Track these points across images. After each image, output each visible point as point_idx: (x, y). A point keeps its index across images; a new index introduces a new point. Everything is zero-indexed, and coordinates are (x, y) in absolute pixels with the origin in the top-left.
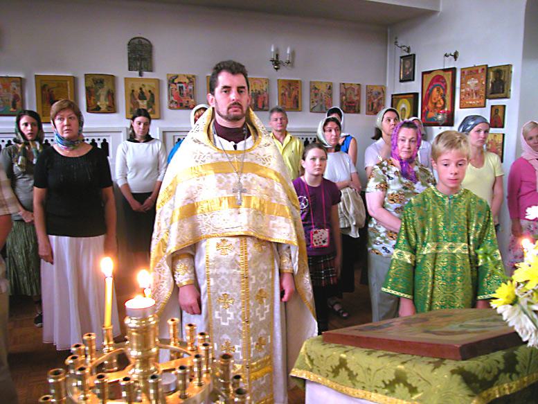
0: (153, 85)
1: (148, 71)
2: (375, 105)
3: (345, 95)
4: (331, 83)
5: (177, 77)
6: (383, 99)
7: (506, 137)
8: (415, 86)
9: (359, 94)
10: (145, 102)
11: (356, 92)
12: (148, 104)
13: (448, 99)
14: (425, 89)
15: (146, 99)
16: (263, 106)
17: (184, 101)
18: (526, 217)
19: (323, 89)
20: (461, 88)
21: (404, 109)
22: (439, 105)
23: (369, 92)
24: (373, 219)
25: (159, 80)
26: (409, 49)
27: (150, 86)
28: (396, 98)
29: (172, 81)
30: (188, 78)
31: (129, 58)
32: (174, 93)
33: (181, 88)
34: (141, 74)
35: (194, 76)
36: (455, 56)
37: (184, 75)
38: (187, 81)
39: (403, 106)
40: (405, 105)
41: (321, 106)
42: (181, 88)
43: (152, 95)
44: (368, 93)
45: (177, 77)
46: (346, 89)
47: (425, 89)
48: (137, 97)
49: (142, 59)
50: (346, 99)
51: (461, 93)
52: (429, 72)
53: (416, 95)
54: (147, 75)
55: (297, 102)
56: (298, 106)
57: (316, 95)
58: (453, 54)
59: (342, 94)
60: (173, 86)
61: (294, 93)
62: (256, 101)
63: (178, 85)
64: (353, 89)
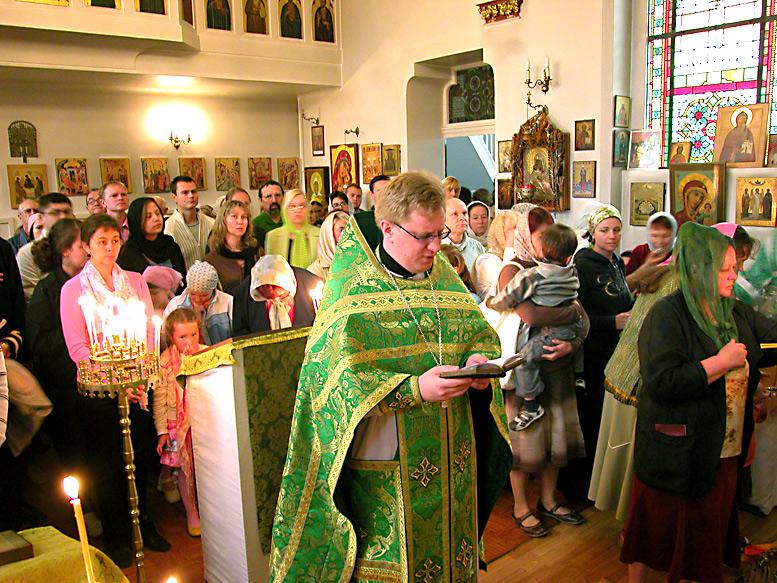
0: (41, 171)
1: (33, 156)
2: (288, 180)
3: (255, 170)
4: (238, 159)
5: (67, 161)
6: (297, 171)
7: (612, 123)
8: (325, 162)
9: (269, 169)
10: (33, 190)
11: (266, 167)
12: (36, 192)
13: (353, 174)
14: (334, 163)
15: (33, 187)
16: (165, 187)
17: (77, 187)
18: (36, 398)
19: (230, 166)
20: (364, 164)
21: (316, 183)
22: (346, 180)
23: (281, 165)
24: (174, 346)
25: (45, 166)
26: (318, 121)
27: (36, 172)
28: (309, 171)
29: (61, 166)
30: (80, 163)
31: (11, 144)
32: (65, 179)
33: (72, 173)
34: (25, 161)
35: (85, 160)
36: (357, 132)
37: (74, 159)
38: (79, 165)
39: (316, 180)
40: (317, 178)
41: (229, 183)
42: (72, 173)
43: (40, 183)
44: (279, 166)
45: (67, 161)
46: (255, 165)
47: (334, 163)
48: (23, 185)
49: (24, 143)
50: (256, 175)
51: (363, 169)
52: (336, 147)
53: (326, 169)
54: (31, 160)
55: (202, 181)
56: (203, 186)
57: (222, 172)
58: (354, 130)
59: (251, 170)
60: (62, 171)
61: (198, 172)
62: (156, 183)
63: (69, 170)
64: (263, 164)
